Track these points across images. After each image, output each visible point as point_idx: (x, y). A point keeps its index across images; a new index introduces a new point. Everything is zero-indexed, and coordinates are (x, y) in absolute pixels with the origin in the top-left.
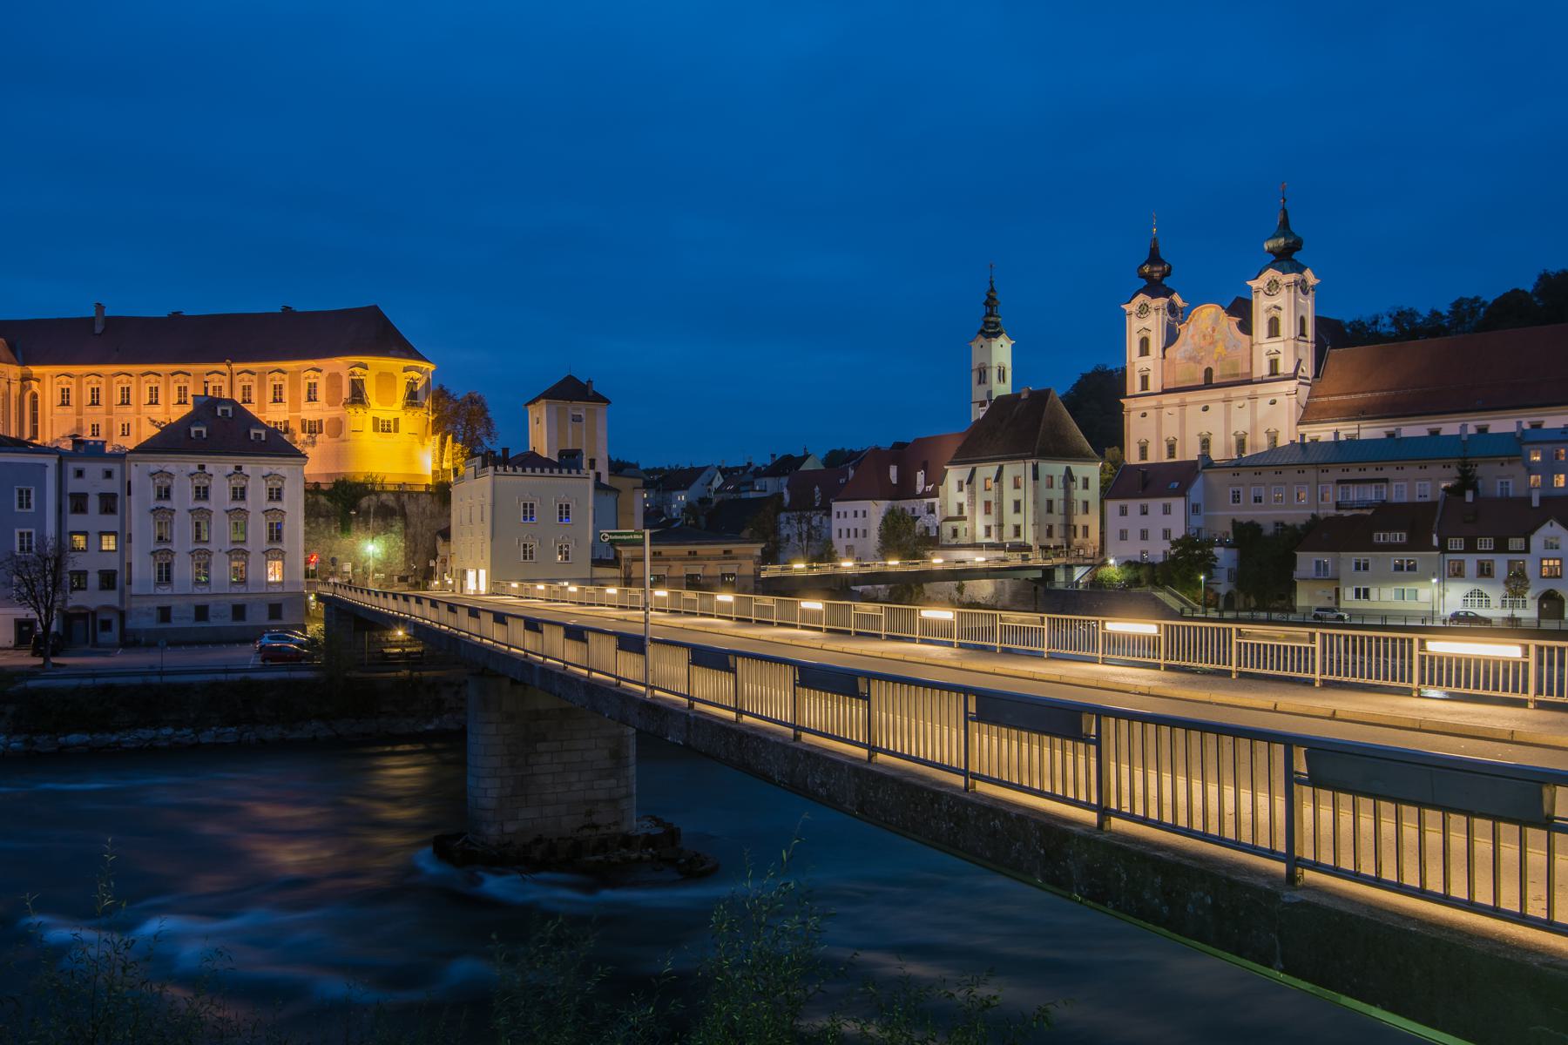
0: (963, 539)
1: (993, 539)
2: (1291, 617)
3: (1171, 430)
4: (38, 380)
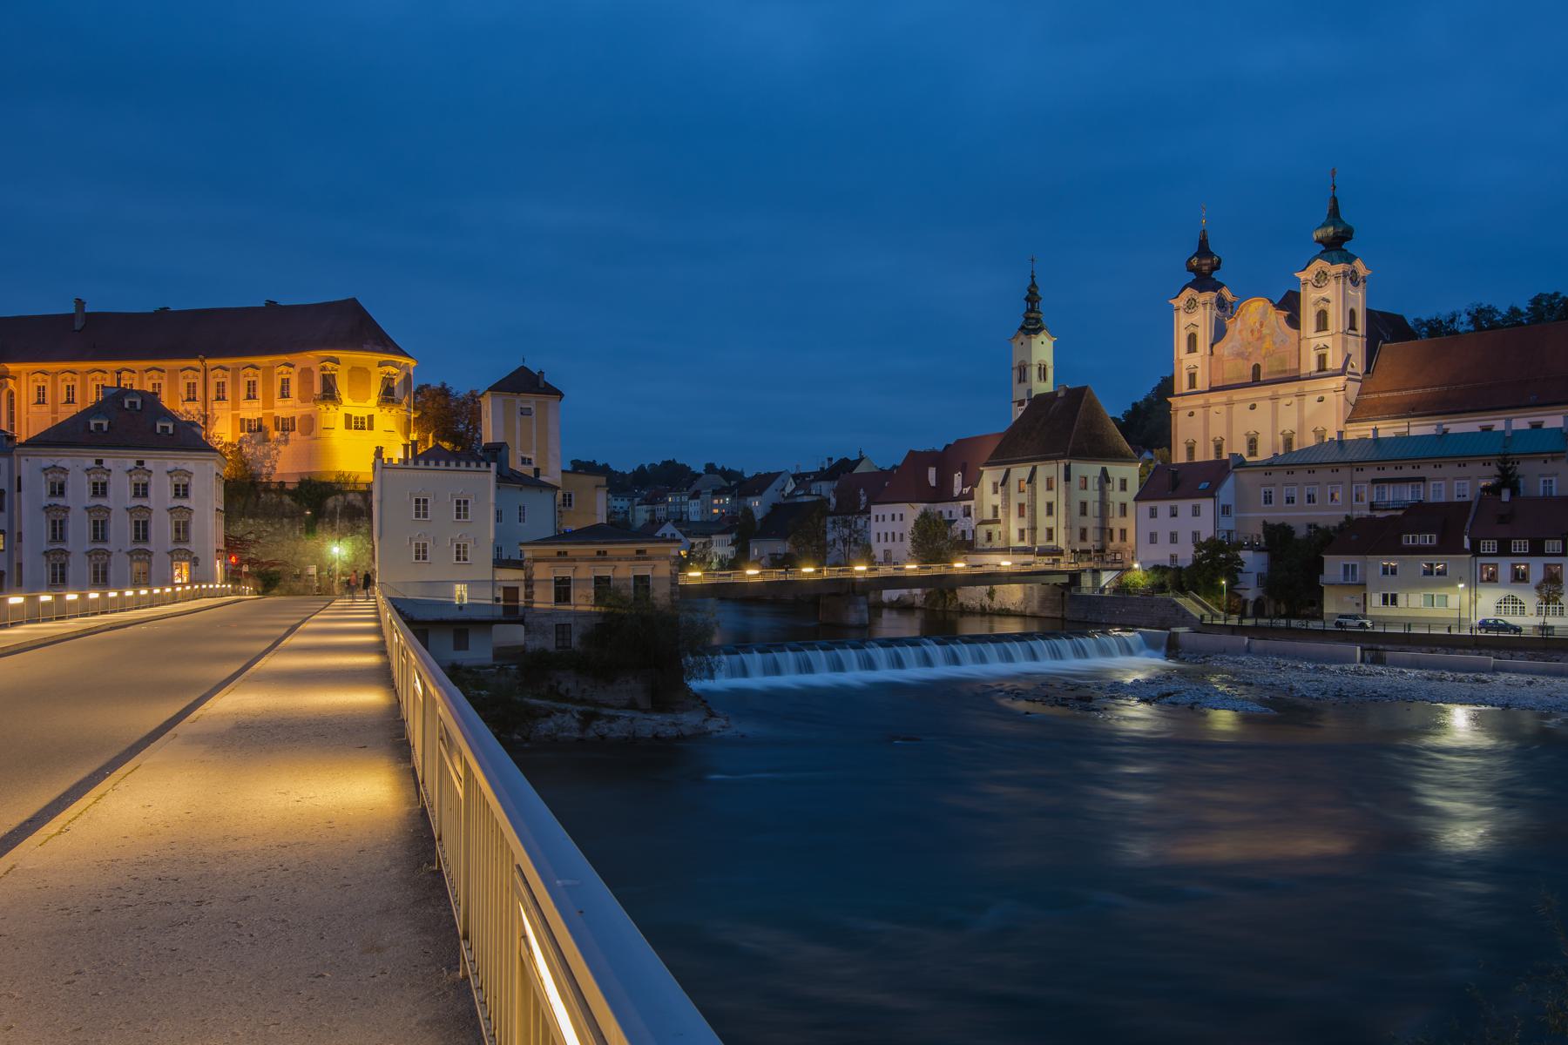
0: (997, 543)
1: (1026, 544)
2: (1314, 625)
3: (1218, 430)
4: (14, 378)
